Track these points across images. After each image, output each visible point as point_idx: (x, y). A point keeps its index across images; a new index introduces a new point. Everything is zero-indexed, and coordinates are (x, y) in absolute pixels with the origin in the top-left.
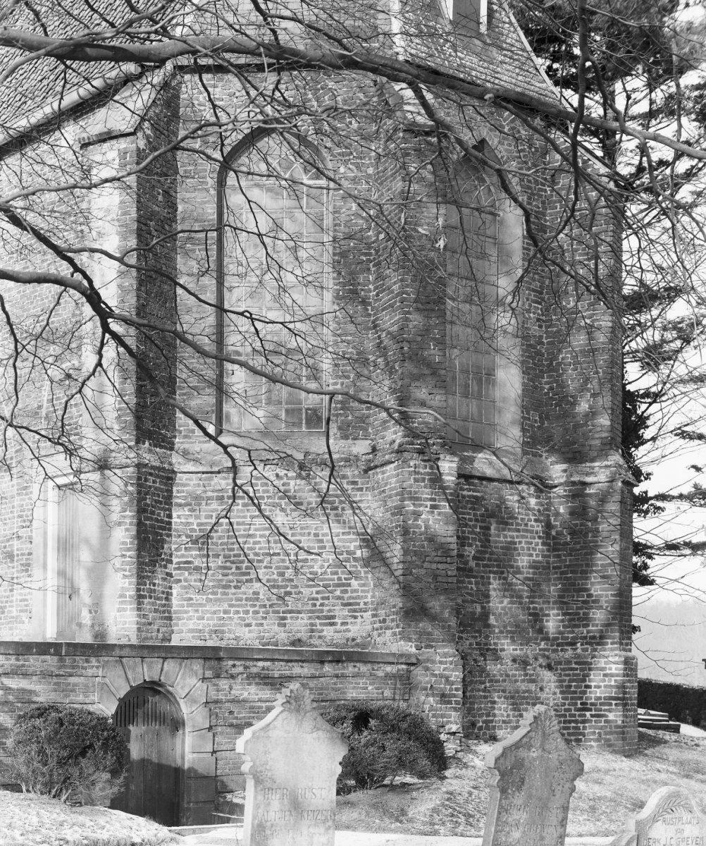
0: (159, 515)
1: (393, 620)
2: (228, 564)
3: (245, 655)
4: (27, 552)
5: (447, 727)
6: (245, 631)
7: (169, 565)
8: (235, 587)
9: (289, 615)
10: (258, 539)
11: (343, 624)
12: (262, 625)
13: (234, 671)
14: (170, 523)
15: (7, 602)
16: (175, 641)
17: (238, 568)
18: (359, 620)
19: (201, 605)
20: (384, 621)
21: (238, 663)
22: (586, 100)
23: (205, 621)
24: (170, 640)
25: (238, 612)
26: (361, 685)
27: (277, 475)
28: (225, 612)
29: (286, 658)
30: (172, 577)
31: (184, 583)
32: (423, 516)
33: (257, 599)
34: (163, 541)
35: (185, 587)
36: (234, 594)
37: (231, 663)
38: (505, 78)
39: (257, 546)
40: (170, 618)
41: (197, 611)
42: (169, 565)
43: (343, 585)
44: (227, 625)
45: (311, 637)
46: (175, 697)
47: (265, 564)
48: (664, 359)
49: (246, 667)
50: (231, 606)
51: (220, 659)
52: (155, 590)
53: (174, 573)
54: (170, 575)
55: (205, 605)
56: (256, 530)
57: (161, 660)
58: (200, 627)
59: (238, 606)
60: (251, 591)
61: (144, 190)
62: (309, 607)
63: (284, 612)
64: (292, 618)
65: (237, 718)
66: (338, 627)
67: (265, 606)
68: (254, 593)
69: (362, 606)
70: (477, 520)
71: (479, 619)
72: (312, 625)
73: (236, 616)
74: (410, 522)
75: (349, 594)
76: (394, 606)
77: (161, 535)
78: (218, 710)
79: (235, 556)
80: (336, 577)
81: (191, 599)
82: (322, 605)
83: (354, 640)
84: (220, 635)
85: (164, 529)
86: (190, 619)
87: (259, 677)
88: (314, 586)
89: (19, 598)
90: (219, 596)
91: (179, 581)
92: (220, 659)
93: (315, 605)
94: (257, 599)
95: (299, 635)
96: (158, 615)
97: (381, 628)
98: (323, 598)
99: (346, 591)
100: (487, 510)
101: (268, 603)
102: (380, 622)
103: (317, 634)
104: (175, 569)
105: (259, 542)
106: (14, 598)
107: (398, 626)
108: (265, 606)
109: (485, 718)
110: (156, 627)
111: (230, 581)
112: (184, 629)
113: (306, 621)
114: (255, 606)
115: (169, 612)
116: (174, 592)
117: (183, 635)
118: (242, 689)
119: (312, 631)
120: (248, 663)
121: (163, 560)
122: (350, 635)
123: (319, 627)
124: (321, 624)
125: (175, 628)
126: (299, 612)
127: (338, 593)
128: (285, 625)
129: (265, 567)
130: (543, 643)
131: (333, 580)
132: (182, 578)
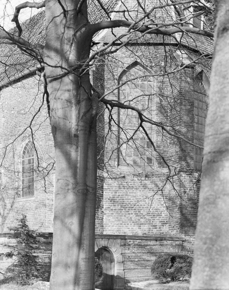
0: (100, 192)
1: (177, 227)
2: (122, 208)
3: (133, 238)
4: (51, 204)
6: (128, 230)
7: (103, 209)
8: (124, 216)
9: (142, 225)
10: (132, 200)
11: (159, 228)
12: (133, 228)
13: (130, 243)
14: (103, 195)
15: (44, 221)
16: (105, 233)
18: (165, 227)
19: (113, 222)
20: (174, 227)
21: (131, 240)
22: (117, 100)
23: (114, 227)
24: (103, 233)
25: (125, 224)
26: (168, 248)
27: (138, 179)
28: (121, 224)
29: (146, 239)
30: (103, 212)
31: (107, 215)
32: (187, 193)
33: (131, 220)
34: (101, 201)
35: (108, 216)
36: (124, 218)
37: (129, 240)
38: (209, 50)
39: (131, 202)
40: (103, 226)
41: (112, 224)
42: (103, 209)
43: (160, 215)
44: (122, 228)
45: (149, 232)
46: (111, 252)
47: (134, 208)
48: (3, 201)
49: (134, 242)
50: (123, 222)
51: (126, 239)
52: (98, 217)
53: (104, 211)
54: (103, 212)
55: (114, 222)
56: (131, 197)
57: (108, 240)
59: (125, 222)
60: (129, 217)
61: (95, 84)
63: (140, 224)
64: (143, 226)
65: (131, 259)
66: (158, 229)
67: (134, 222)
68: (130, 218)
69: (166, 222)
72: (149, 228)
73: (125, 225)
74: (183, 195)
75: (161, 218)
76: (177, 222)
77: (100, 199)
78: (125, 256)
79: (124, 206)
80: (157, 213)
81: (110, 220)
82: (153, 222)
83: (163, 233)
84: (119, 232)
85: (101, 197)
86: (109, 226)
87: (138, 245)
88: (150, 216)
89: (48, 219)
90: (119, 219)
91: (106, 214)
92: (126, 239)
93: (150, 222)
94: (131, 220)
95: (145, 232)
96: (99, 225)
97: (172, 229)
98: (153, 220)
99: (160, 217)
101: (135, 221)
102: (172, 227)
103: (151, 231)
104: (105, 210)
105: (132, 201)
106: (46, 220)
107: (178, 229)
108: (134, 222)
110: (99, 229)
111: (123, 214)
112: (107, 230)
113: (147, 227)
114: (131, 222)
115: (103, 224)
116: (104, 217)
117: (107, 232)
118: (133, 249)
119: (149, 230)
120: (134, 241)
121: (101, 207)
122: (162, 232)
123: (151, 229)
124: (152, 228)
126: (145, 224)
127: (158, 218)
129: (134, 210)
132: (107, 213)
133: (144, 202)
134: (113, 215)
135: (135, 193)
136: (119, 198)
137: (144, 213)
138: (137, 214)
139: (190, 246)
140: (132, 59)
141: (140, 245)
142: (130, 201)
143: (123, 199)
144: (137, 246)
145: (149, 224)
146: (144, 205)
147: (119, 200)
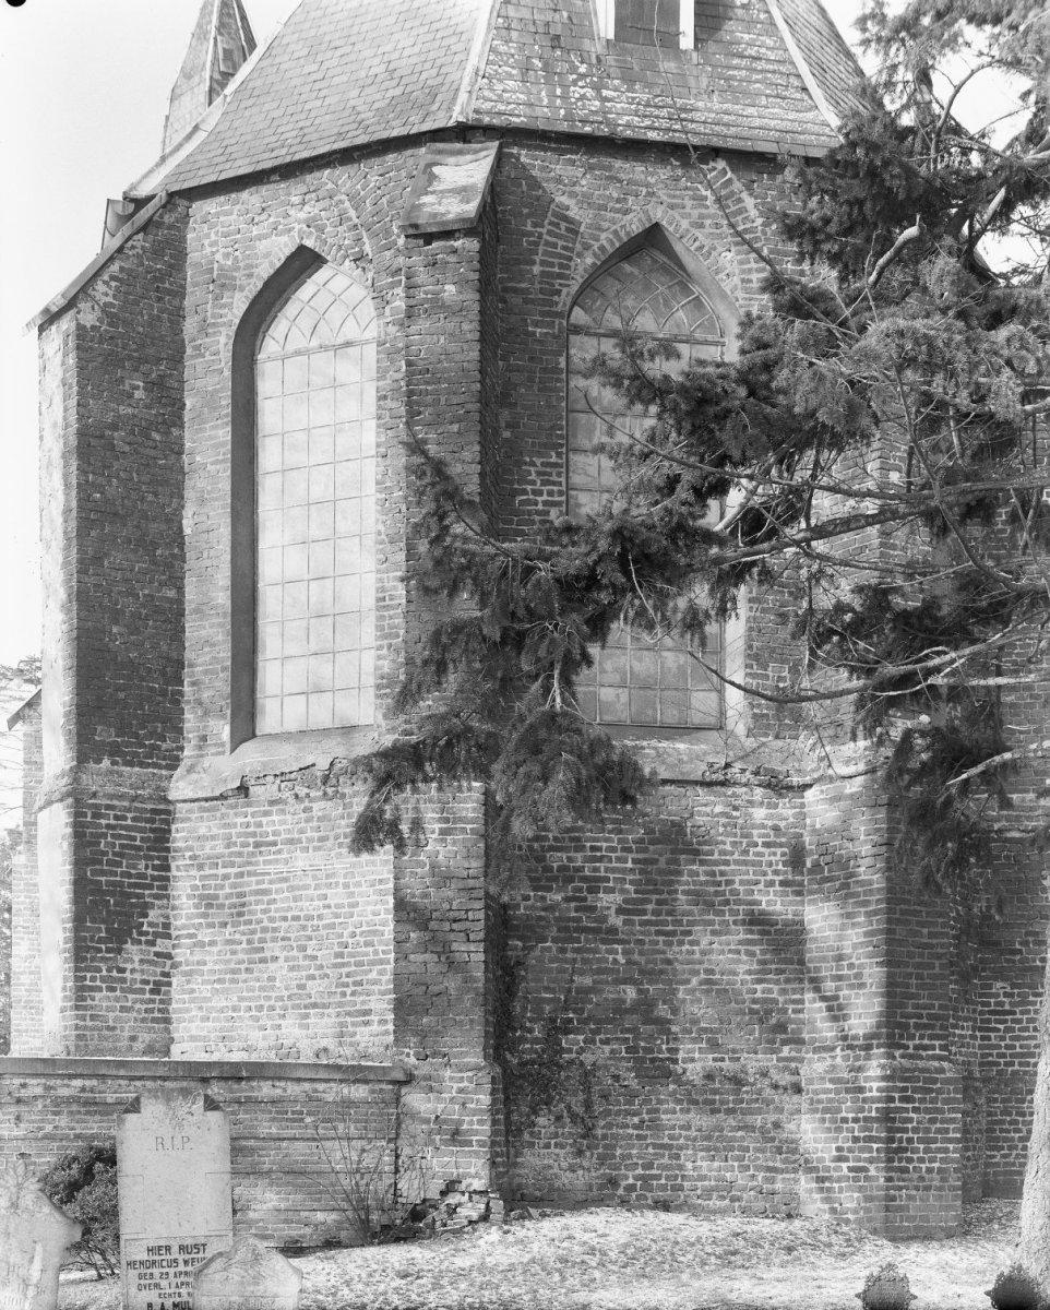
2: (237, 936)
5: (464, 1183)
17: (249, 942)
19: (206, 999)
24: (167, 1053)
28: (235, 1009)
37: (17, 1081)
49: (48, 1088)
50: (241, 999)
56: (271, 882)
58: (204, 1033)
62: (338, 998)
64: (316, 1015)
70: (624, 849)
71: (633, 1010)
72: (342, 1025)
80: (371, 949)
81: (193, 991)
95: (324, 1043)
98: (356, 983)
100: (649, 831)
109: (640, 1171)
114: (269, 998)
120: (52, 1082)
123: (350, 1029)
125: (175, 1035)
126: (325, 1006)
128: (307, 1027)
129: (283, 939)
130: (786, 1049)
131: (367, 954)
133: (321, 903)
134: (205, 968)
135: (287, 862)
136: (228, 890)
137: (319, 954)
138: (295, 958)
139: (441, 1106)
140: (285, 239)
141: (86, 1103)
142: (266, 898)
143: (242, 895)
144: (74, 1108)
145: (340, 1004)
146: (320, 917)
147: (228, 896)
